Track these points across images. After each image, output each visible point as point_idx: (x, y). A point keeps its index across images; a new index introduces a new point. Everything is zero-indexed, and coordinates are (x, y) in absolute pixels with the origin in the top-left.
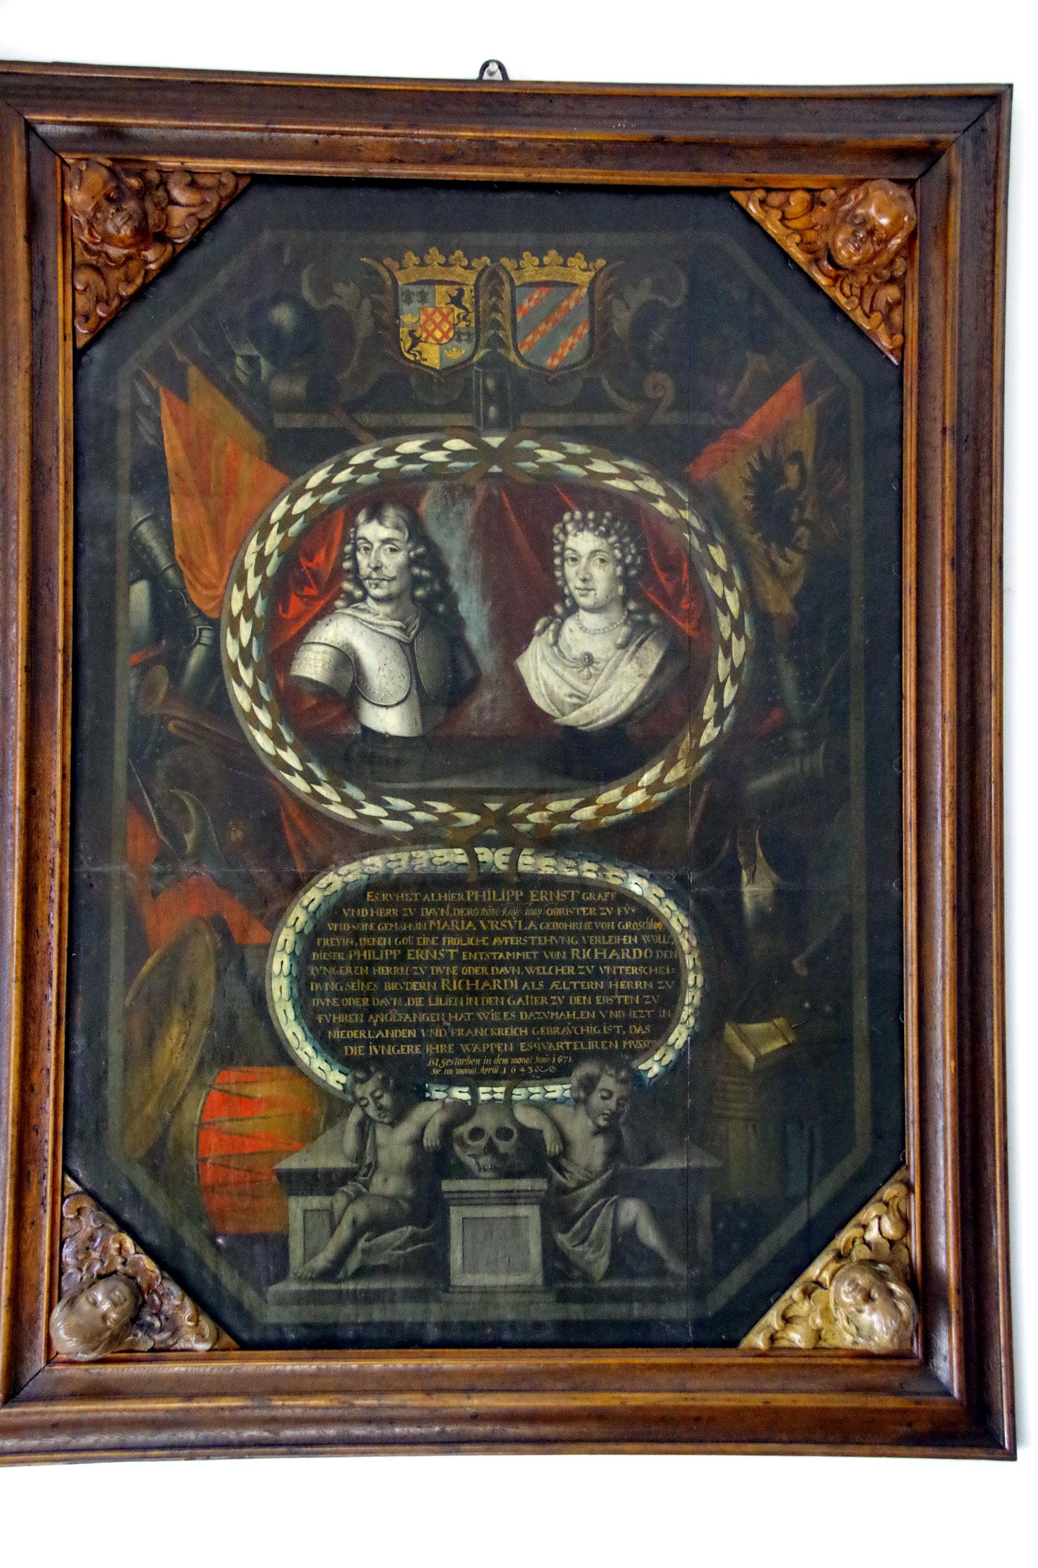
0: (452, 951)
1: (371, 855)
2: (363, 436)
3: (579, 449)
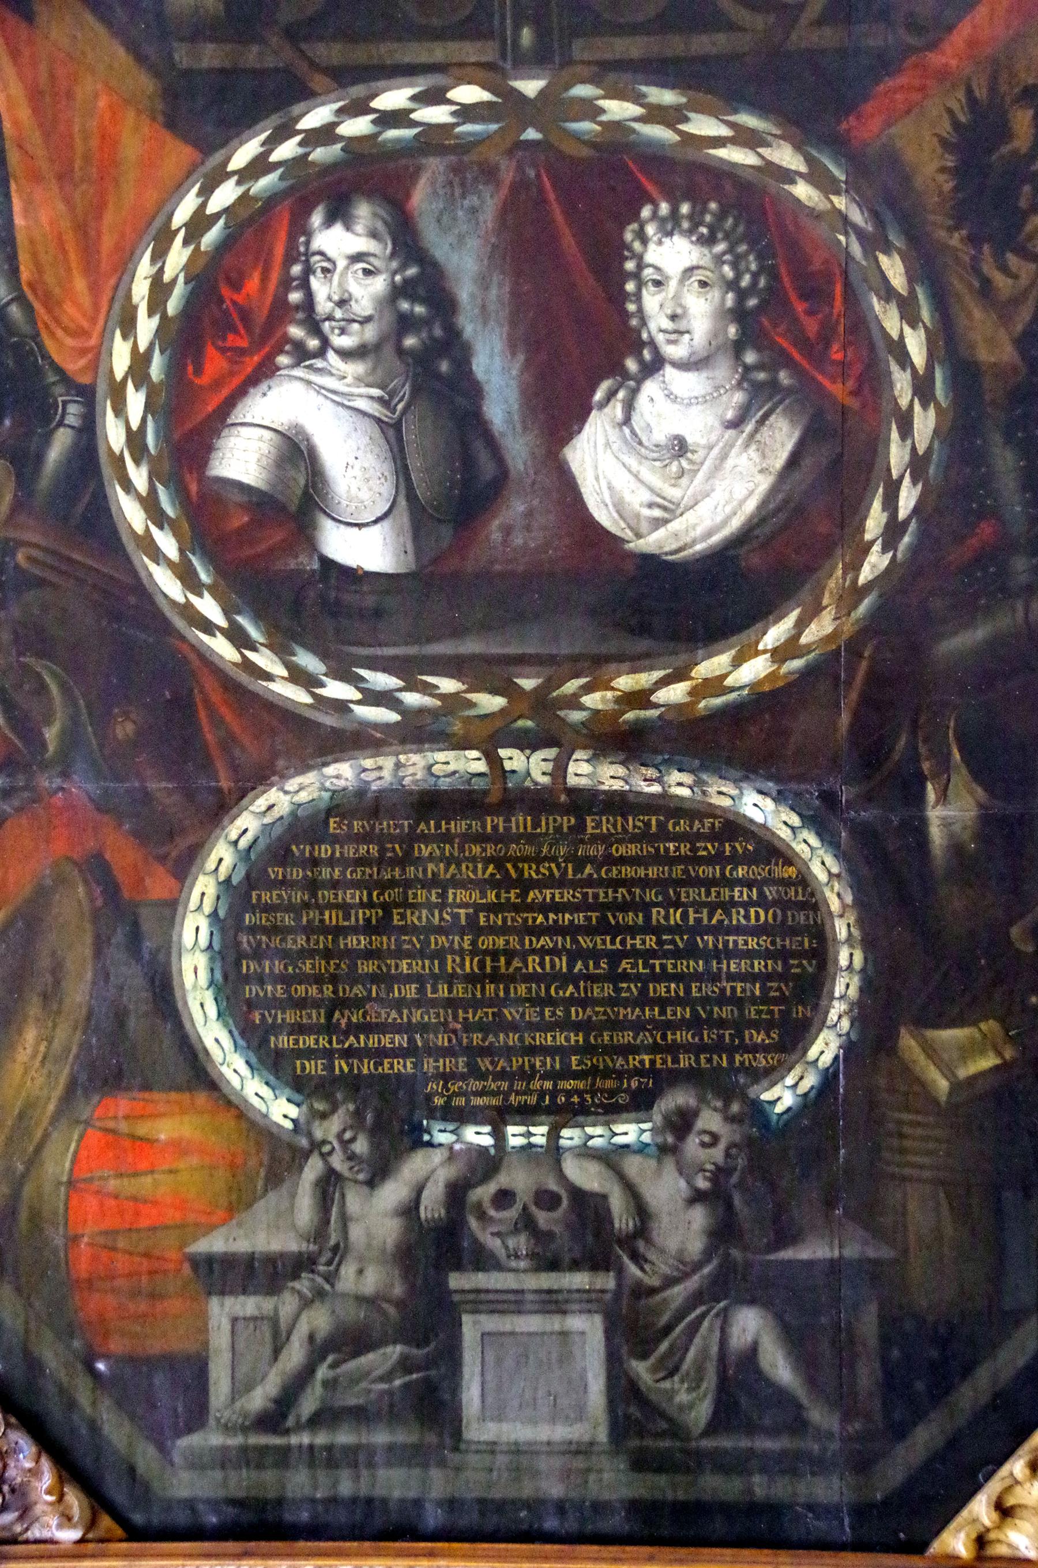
0: (462, 911)
1: (336, 761)
2: (318, 81)
3: (668, 97)
